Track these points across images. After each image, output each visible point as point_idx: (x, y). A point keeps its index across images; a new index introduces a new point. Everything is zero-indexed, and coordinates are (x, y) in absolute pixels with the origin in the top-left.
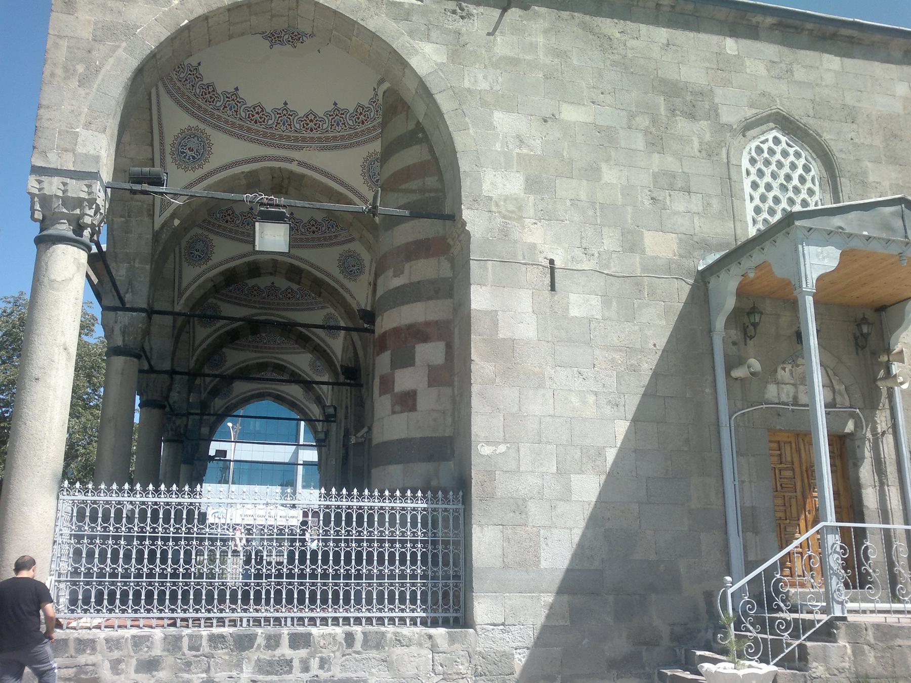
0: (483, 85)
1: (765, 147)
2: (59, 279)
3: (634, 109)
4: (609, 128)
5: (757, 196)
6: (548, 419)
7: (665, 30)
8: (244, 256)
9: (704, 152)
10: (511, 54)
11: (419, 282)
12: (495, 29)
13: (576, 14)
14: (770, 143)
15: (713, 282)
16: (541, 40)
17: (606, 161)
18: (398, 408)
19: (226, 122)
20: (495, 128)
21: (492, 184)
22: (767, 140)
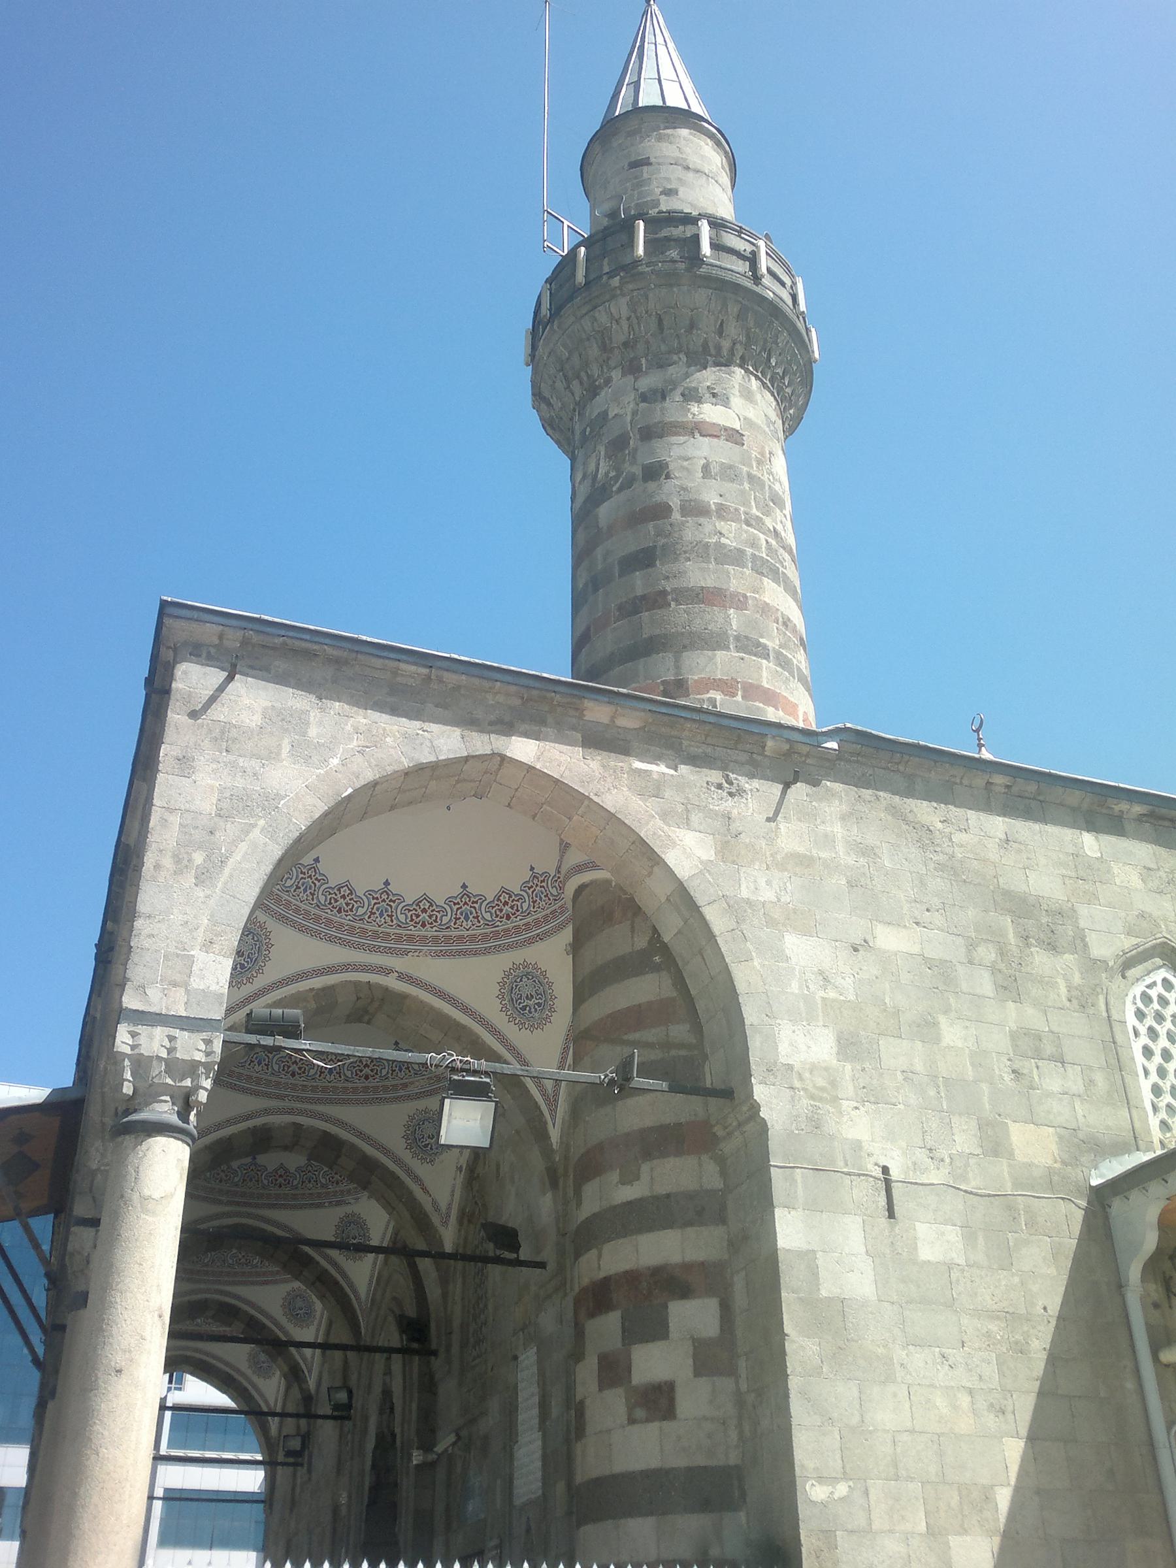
0: (767, 895)
1: (1153, 993)
2: (156, 1196)
3: (973, 935)
4: (943, 962)
5: (1152, 1068)
6: (905, 1437)
7: (1001, 819)
8: (248, 1117)
9: (1075, 1002)
10: (801, 850)
11: (668, 1196)
12: (777, 812)
13: (881, 793)
14: (1159, 989)
15: (1117, 1206)
16: (838, 829)
17: (946, 1012)
18: (640, 1413)
19: (297, 911)
20: (788, 959)
21: (791, 1044)
22: (1154, 984)
